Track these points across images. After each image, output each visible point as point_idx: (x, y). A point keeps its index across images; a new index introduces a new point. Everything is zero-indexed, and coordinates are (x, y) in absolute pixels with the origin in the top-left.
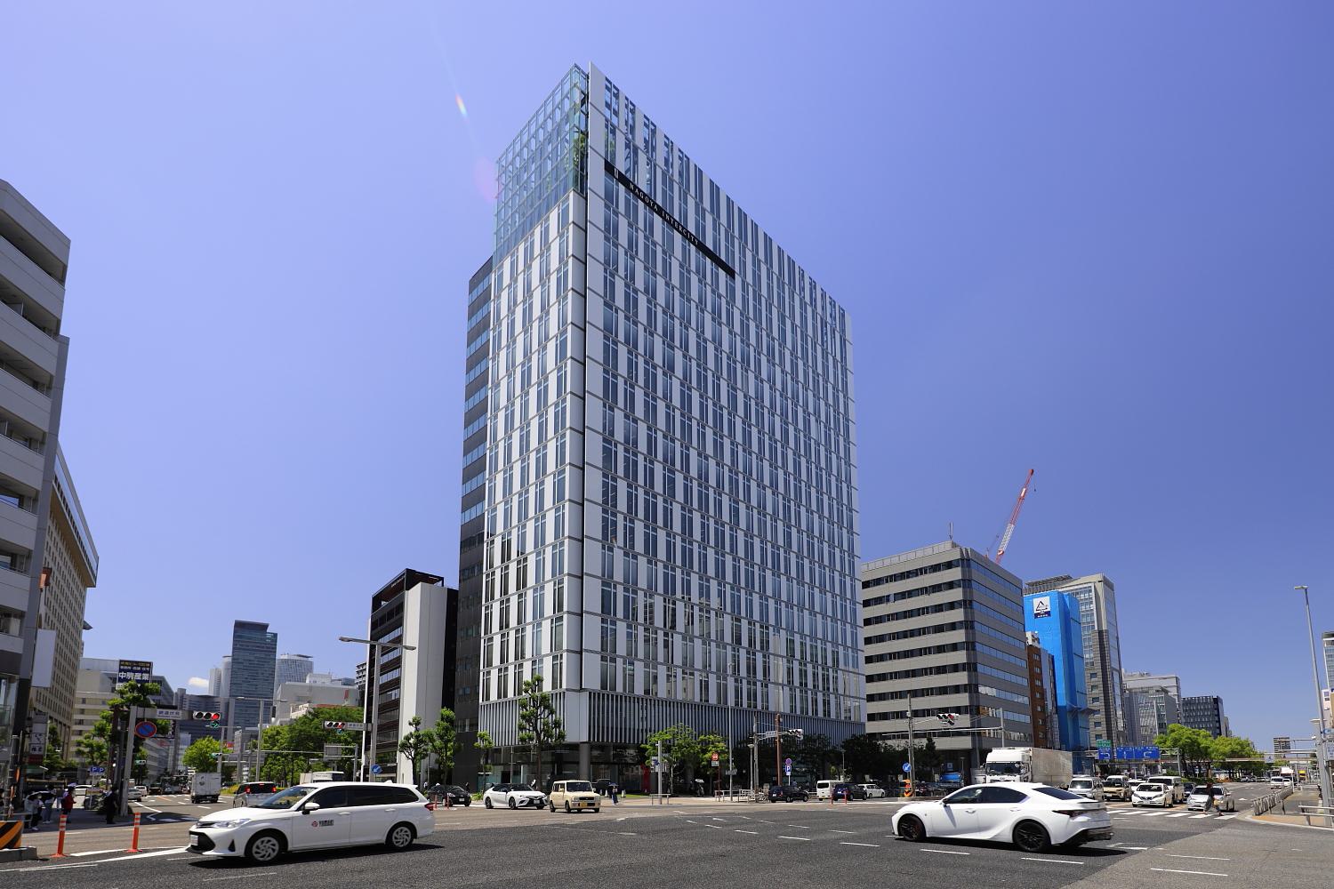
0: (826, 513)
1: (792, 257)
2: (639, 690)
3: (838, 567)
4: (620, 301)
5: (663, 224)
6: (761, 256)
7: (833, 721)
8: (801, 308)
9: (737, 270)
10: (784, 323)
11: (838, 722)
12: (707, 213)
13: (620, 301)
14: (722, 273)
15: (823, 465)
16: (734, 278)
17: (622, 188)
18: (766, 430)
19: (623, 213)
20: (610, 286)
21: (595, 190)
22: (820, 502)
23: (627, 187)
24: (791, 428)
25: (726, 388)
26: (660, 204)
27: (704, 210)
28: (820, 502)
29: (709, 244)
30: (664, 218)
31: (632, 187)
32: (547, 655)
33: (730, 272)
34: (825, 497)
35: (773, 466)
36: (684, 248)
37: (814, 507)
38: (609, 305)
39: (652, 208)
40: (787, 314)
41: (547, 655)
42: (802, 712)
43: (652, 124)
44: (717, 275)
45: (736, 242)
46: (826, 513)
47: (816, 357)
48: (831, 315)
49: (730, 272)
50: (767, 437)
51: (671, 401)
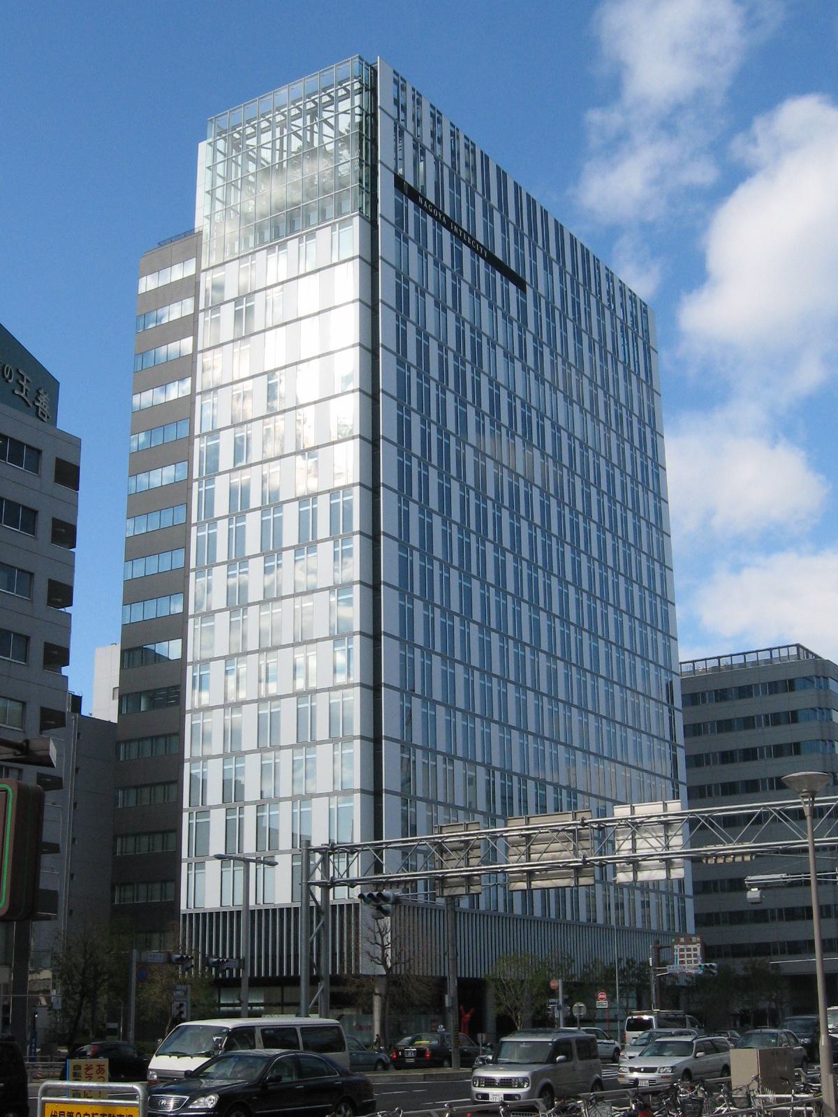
0: (525, 553)
1: (502, 168)
2: (583, 917)
3: (477, 615)
4: (412, 357)
5: (452, 239)
6: (553, 255)
7: (537, 921)
8: (485, 215)
9: (528, 280)
10: (580, 341)
11: (544, 921)
12: (497, 207)
13: (412, 357)
14: (512, 287)
15: (451, 426)
16: (524, 290)
17: (411, 204)
18: (434, 417)
19: (413, 238)
20: (401, 336)
21: (386, 217)
22: (445, 495)
23: (415, 201)
24: (471, 411)
25: (453, 404)
26: (448, 215)
27: (492, 208)
28: (445, 495)
29: (499, 254)
30: (452, 232)
31: (421, 200)
32: (217, 807)
33: (521, 284)
34: (455, 486)
35: (444, 475)
36: (473, 264)
37: (434, 504)
38: (401, 362)
39: (440, 222)
40: (583, 327)
41: (217, 807)
42: (558, 915)
43: (402, 79)
44: (508, 290)
45: (526, 240)
46: (525, 553)
47: (566, 338)
48: (467, 165)
49: (521, 284)
50: (434, 428)
51: (465, 480)
